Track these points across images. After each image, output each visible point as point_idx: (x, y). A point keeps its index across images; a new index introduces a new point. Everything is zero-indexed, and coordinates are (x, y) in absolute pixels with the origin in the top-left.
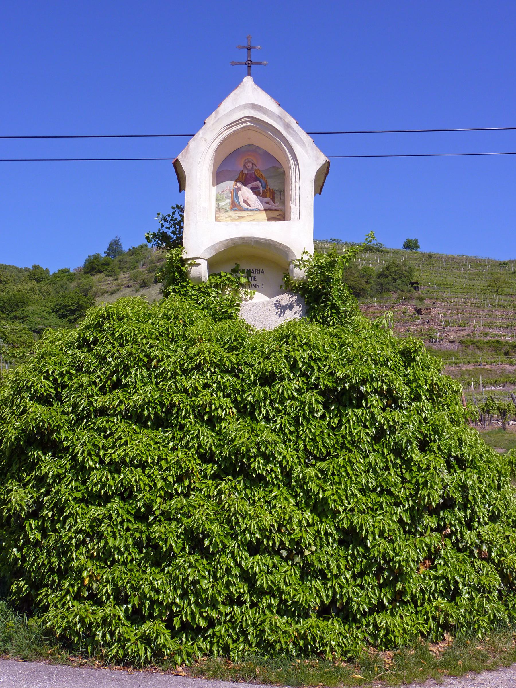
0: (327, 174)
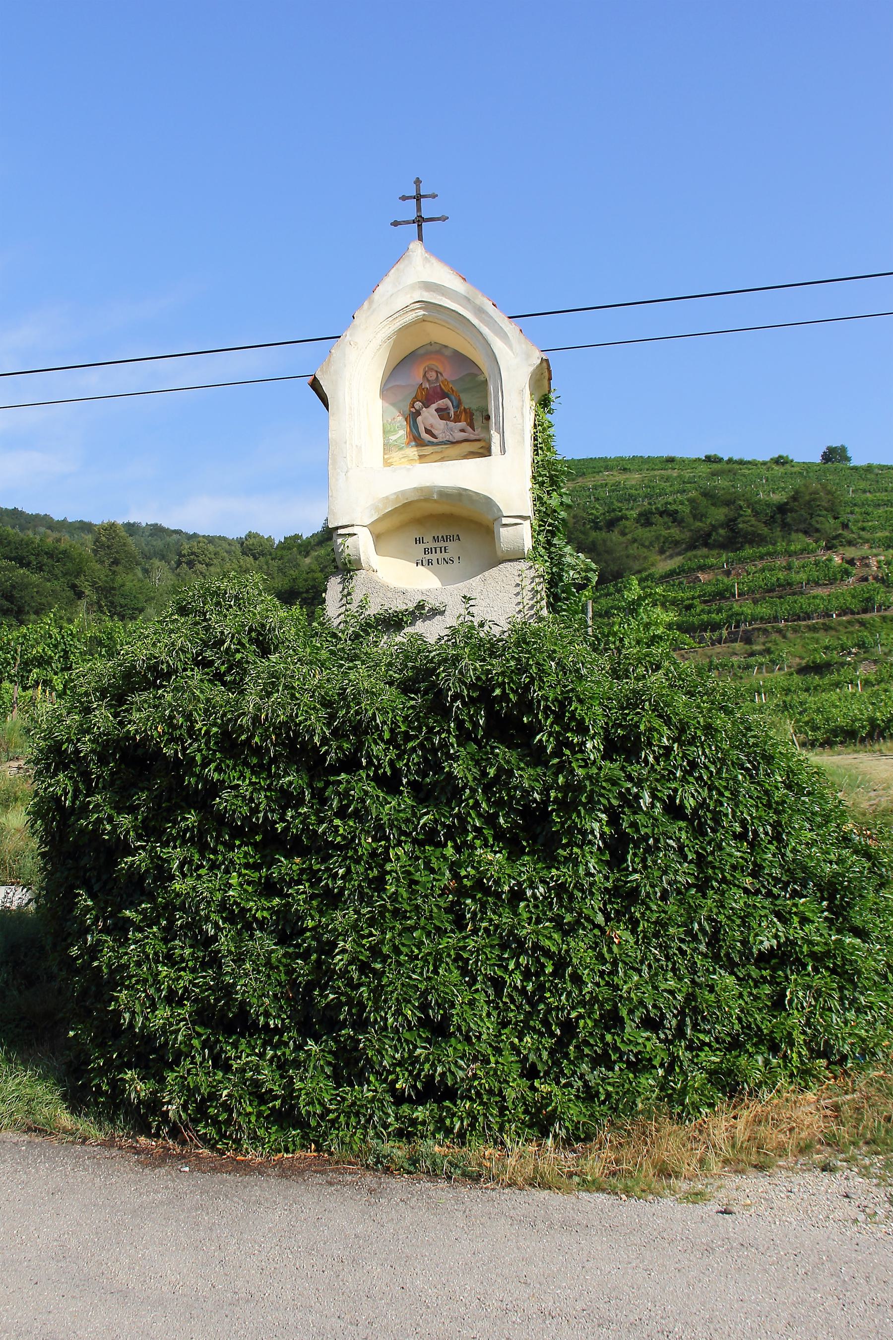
0: (550, 379)
